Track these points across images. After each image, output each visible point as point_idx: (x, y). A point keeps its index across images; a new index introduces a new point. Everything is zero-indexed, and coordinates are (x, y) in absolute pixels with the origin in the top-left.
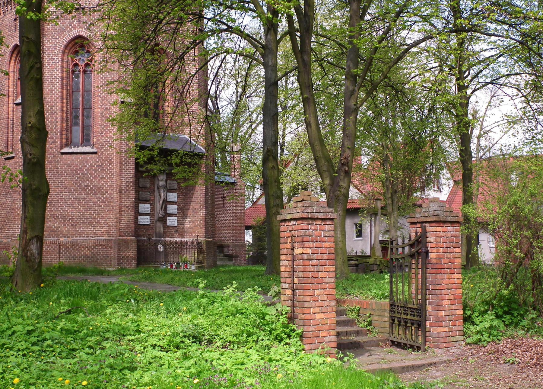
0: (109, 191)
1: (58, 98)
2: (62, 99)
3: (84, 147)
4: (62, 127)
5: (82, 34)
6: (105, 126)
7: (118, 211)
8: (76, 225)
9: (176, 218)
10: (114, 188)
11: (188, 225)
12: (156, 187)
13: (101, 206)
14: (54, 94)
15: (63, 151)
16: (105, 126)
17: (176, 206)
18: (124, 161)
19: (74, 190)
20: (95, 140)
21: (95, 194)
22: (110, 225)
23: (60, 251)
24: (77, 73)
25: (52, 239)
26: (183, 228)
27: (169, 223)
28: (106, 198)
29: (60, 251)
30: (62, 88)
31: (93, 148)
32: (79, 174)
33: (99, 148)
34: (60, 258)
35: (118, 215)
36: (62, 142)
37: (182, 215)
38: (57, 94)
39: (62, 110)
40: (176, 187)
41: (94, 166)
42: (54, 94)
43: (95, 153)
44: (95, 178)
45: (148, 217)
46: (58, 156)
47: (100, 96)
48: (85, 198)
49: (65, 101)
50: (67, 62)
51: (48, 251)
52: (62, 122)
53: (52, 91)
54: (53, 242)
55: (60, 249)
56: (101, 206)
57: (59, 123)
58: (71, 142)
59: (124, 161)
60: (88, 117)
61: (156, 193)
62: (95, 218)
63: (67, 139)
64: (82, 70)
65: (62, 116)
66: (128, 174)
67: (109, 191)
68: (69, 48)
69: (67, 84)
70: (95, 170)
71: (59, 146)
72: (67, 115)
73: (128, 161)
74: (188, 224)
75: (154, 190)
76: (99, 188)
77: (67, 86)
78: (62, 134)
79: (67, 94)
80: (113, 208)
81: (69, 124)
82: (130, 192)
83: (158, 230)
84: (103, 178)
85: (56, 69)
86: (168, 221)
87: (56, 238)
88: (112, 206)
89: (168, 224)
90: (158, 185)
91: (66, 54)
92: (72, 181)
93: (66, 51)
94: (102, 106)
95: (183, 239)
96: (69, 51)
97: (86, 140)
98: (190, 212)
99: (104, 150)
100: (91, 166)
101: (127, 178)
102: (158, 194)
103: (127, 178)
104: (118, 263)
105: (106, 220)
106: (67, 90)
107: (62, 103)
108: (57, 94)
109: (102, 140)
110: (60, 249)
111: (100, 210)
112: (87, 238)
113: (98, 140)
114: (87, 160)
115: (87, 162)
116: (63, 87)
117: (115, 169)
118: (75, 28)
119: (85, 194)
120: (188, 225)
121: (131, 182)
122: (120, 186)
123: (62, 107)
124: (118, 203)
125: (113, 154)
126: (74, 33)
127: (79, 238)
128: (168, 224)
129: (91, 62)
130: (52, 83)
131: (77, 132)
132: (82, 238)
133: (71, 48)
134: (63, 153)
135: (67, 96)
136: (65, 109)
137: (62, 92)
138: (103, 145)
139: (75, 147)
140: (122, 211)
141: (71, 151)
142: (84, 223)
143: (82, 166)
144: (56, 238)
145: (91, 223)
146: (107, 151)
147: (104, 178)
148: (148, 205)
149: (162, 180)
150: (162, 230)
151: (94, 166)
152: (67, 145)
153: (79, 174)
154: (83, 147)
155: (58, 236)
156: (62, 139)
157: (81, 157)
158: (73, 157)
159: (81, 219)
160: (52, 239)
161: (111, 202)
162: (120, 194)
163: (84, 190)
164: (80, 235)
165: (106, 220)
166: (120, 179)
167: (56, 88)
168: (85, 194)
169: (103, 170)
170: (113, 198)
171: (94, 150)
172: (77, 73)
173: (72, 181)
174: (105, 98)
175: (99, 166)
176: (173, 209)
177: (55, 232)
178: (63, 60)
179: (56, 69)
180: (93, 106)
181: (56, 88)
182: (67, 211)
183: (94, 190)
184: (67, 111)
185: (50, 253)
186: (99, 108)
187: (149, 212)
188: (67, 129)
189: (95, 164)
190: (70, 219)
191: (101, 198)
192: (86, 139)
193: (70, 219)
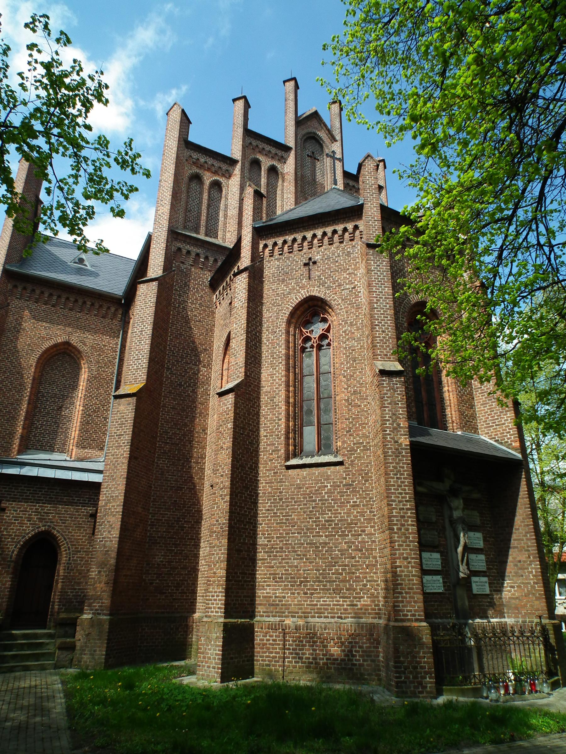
0: (368, 530)
1: (280, 385)
2: (288, 386)
3: (322, 456)
4: (287, 427)
5: (313, 294)
6: (353, 419)
7: (389, 566)
8: (312, 594)
9: (485, 579)
10: (375, 523)
11: (510, 591)
12: (447, 521)
13: (354, 558)
14: (275, 380)
15: (288, 463)
16: (353, 419)
17: (482, 557)
18: (391, 471)
19: (308, 529)
20: (339, 444)
21: (344, 535)
22: (372, 594)
23: (284, 645)
24: (308, 350)
25: (271, 619)
26: (501, 598)
27: (476, 589)
28: (363, 542)
29: (284, 645)
30: (288, 370)
31: (336, 456)
32: (315, 501)
33: (345, 455)
34: (284, 658)
35: (389, 575)
36: (287, 450)
37: (497, 573)
38: (281, 379)
39: (288, 403)
40: (478, 521)
41: (339, 486)
42: (275, 380)
43: (341, 463)
44: (342, 505)
45: (439, 578)
46: (281, 473)
47: (343, 374)
48: (326, 543)
49: (291, 389)
50: (295, 336)
51: (264, 644)
52: (288, 420)
53: (272, 375)
54: (273, 627)
55: (285, 640)
56: (354, 558)
57: (283, 420)
58: (302, 451)
59: (391, 471)
60: (327, 411)
61: (449, 533)
62: (344, 581)
63: (295, 446)
64: (315, 345)
65: (288, 411)
66: (401, 494)
67: (368, 530)
68: (296, 316)
69: (295, 365)
70: (342, 493)
71: (283, 456)
72: (295, 410)
73: (400, 471)
74: (509, 590)
75: (444, 528)
76: (348, 524)
77: (295, 368)
78: (287, 438)
79: (295, 379)
80: (376, 561)
81: (298, 422)
82: (408, 529)
83: (459, 604)
84: (355, 506)
85: (278, 344)
86: (474, 585)
87: (278, 619)
88: (375, 557)
89: (475, 591)
90: (451, 516)
91: (292, 325)
92: (304, 512)
93: (293, 320)
94: (347, 389)
95: (503, 620)
96: (297, 322)
97: (323, 446)
98: (510, 568)
99: (355, 458)
100: (335, 486)
101: (400, 502)
102: (452, 534)
103: (400, 502)
104: (397, 683)
105: (365, 585)
106: (295, 374)
107: (288, 391)
108: (281, 379)
109: (350, 441)
110: (285, 640)
111: (352, 566)
112: (333, 620)
113: (344, 442)
114: (328, 476)
115: (328, 478)
116: (289, 370)
117: (376, 487)
118: (303, 287)
119: (326, 536)
120: (510, 591)
121: (408, 509)
122: (389, 517)
123: (288, 397)
124: (387, 551)
125: (370, 463)
126: (303, 294)
127: (317, 620)
128: (475, 591)
129: (329, 332)
130: (272, 365)
131: (310, 434)
132: (323, 620)
133: (299, 318)
134: (289, 467)
135: (295, 382)
136: (291, 400)
137: (287, 376)
138: (352, 450)
139: (307, 456)
140: (397, 567)
141: (301, 462)
142: (326, 590)
143: (319, 487)
144: (278, 619)
145: (337, 591)
146: (359, 458)
147: (358, 506)
148: (437, 556)
149: (457, 509)
150: (467, 603)
151: (339, 486)
152: (295, 456)
153: (315, 501)
154: (320, 456)
155: (281, 614)
156: (287, 445)
157: (316, 471)
158: (305, 472)
159: (319, 581)
160: (271, 619)
161: (372, 549)
162: (390, 534)
163: (324, 528)
164: (320, 614)
165: (365, 585)
166: (388, 505)
167: (278, 371)
168: (326, 536)
169: (354, 491)
170: (374, 541)
171: (339, 459)
172: (308, 350)
173: (304, 512)
174: (351, 376)
175: (348, 485)
176: (479, 561)
177: (276, 607)
178: (288, 332)
179: (278, 344)
180: (333, 393)
181: (278, 371)
182: (297, 567)
183: (341, 528)
184: (295, 404)
185: (268, 649)
186: (343, 392)
187: (440, 568)
188: (294, 431)
189: (342, 482)
190: (301, 582)
191: (353, 543)
192: (325, 444)
193: (301, 582)
